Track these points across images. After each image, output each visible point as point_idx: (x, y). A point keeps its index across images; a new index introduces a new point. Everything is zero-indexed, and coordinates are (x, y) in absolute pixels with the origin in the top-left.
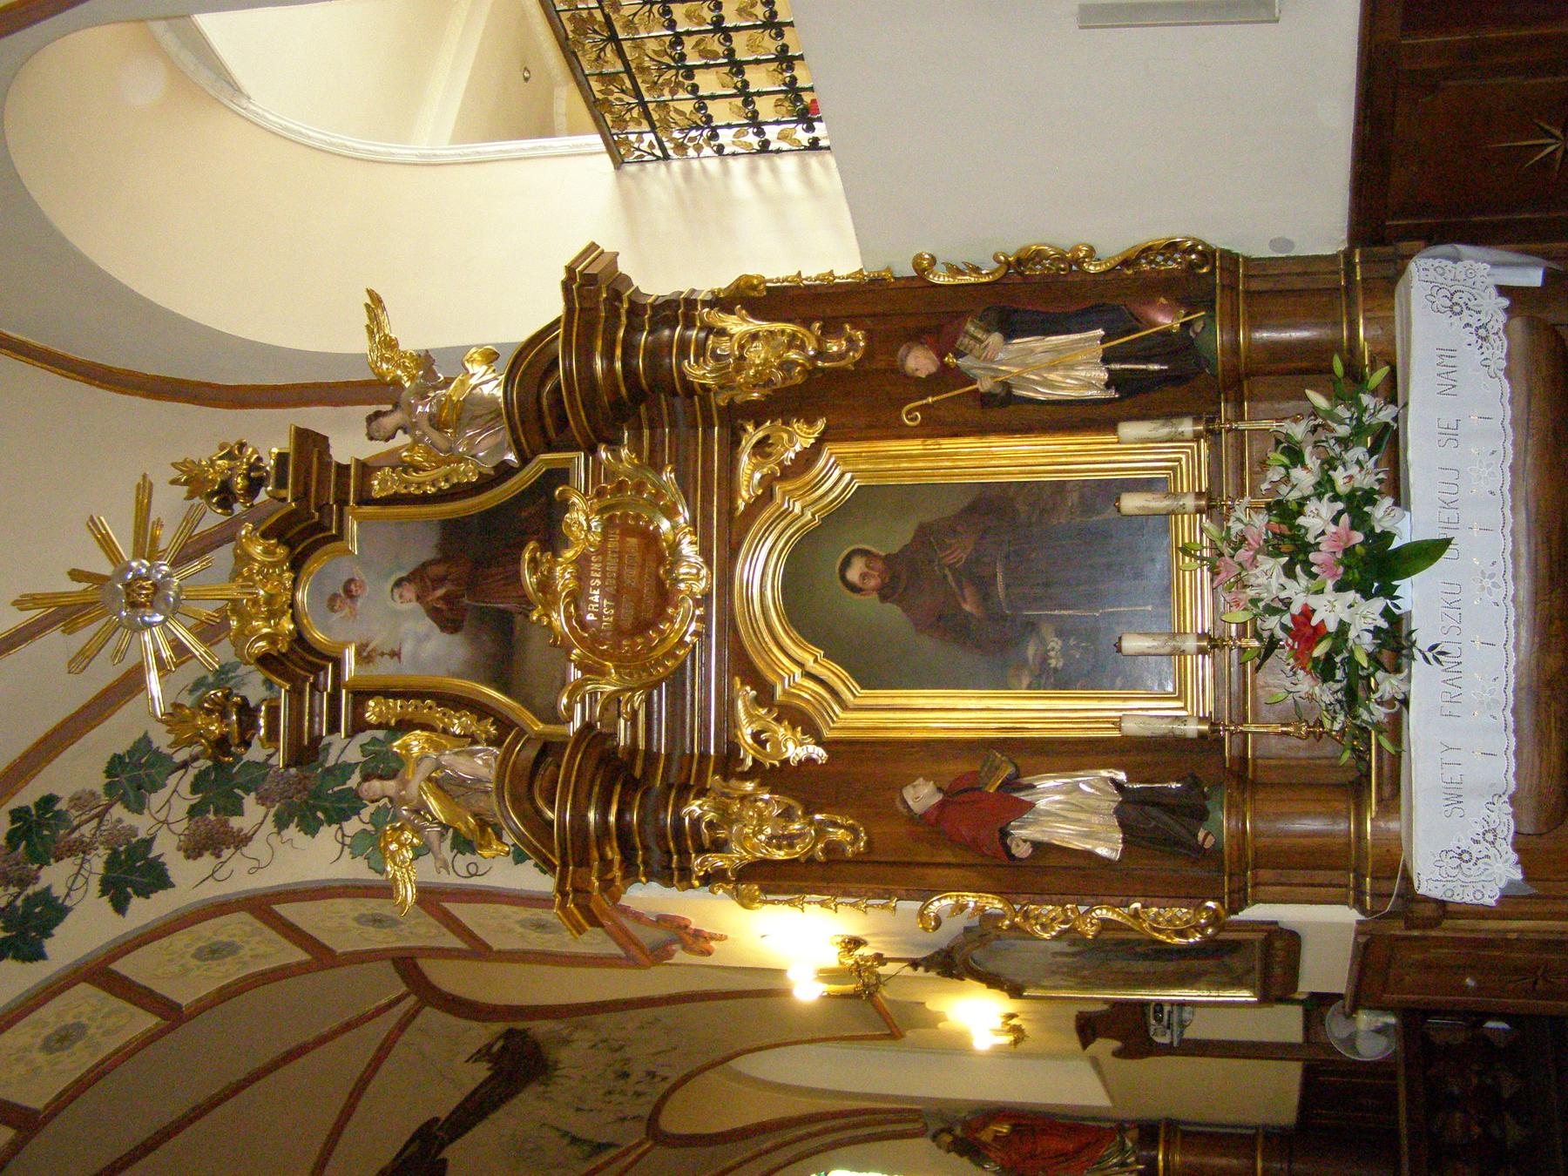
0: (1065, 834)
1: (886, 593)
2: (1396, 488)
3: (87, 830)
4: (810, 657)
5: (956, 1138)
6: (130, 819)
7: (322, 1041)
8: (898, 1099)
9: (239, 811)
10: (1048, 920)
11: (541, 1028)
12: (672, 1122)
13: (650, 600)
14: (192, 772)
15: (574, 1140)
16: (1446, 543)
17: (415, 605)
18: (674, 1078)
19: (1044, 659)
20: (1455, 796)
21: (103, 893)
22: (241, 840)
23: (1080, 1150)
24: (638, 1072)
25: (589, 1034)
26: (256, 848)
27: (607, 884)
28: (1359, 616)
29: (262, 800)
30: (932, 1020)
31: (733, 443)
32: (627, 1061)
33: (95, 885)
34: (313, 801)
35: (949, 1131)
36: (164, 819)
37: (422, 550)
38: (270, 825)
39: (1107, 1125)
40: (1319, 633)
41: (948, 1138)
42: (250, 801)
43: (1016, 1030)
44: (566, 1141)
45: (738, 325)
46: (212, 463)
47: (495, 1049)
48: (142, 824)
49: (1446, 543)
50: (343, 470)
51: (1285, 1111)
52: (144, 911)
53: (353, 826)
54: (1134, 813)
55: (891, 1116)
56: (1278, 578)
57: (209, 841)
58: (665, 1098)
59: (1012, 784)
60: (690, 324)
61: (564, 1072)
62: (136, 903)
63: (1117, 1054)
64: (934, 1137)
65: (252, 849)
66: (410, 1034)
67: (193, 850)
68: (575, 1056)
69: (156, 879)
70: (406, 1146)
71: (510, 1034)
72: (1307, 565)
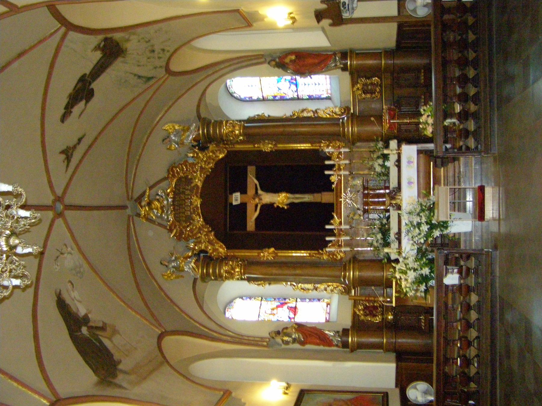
5: (276, 63)
7: (31, 48)
8: (256, 51)
11: (117, 36)
12: (174, 67)
15: (139, 77)
18: (172, 50)
23: (319, 63)
24: (157, 48)
25: (135, 37)
30: (261, 19)
32: (153, 46)
35: (274, 60)
39: (330, 53)
41: (273, 63)
43: (293, 18)
44: (136, 77)
47: (102, 45)
51: (392, 43)
55: (253, 58)
58: (169, 59)
61: (130, 52)
63: (331, 25)
64: (269, 63)
66: (66, 42)
68: (133, 45)
70: (77, 84)
71: (106, 39)
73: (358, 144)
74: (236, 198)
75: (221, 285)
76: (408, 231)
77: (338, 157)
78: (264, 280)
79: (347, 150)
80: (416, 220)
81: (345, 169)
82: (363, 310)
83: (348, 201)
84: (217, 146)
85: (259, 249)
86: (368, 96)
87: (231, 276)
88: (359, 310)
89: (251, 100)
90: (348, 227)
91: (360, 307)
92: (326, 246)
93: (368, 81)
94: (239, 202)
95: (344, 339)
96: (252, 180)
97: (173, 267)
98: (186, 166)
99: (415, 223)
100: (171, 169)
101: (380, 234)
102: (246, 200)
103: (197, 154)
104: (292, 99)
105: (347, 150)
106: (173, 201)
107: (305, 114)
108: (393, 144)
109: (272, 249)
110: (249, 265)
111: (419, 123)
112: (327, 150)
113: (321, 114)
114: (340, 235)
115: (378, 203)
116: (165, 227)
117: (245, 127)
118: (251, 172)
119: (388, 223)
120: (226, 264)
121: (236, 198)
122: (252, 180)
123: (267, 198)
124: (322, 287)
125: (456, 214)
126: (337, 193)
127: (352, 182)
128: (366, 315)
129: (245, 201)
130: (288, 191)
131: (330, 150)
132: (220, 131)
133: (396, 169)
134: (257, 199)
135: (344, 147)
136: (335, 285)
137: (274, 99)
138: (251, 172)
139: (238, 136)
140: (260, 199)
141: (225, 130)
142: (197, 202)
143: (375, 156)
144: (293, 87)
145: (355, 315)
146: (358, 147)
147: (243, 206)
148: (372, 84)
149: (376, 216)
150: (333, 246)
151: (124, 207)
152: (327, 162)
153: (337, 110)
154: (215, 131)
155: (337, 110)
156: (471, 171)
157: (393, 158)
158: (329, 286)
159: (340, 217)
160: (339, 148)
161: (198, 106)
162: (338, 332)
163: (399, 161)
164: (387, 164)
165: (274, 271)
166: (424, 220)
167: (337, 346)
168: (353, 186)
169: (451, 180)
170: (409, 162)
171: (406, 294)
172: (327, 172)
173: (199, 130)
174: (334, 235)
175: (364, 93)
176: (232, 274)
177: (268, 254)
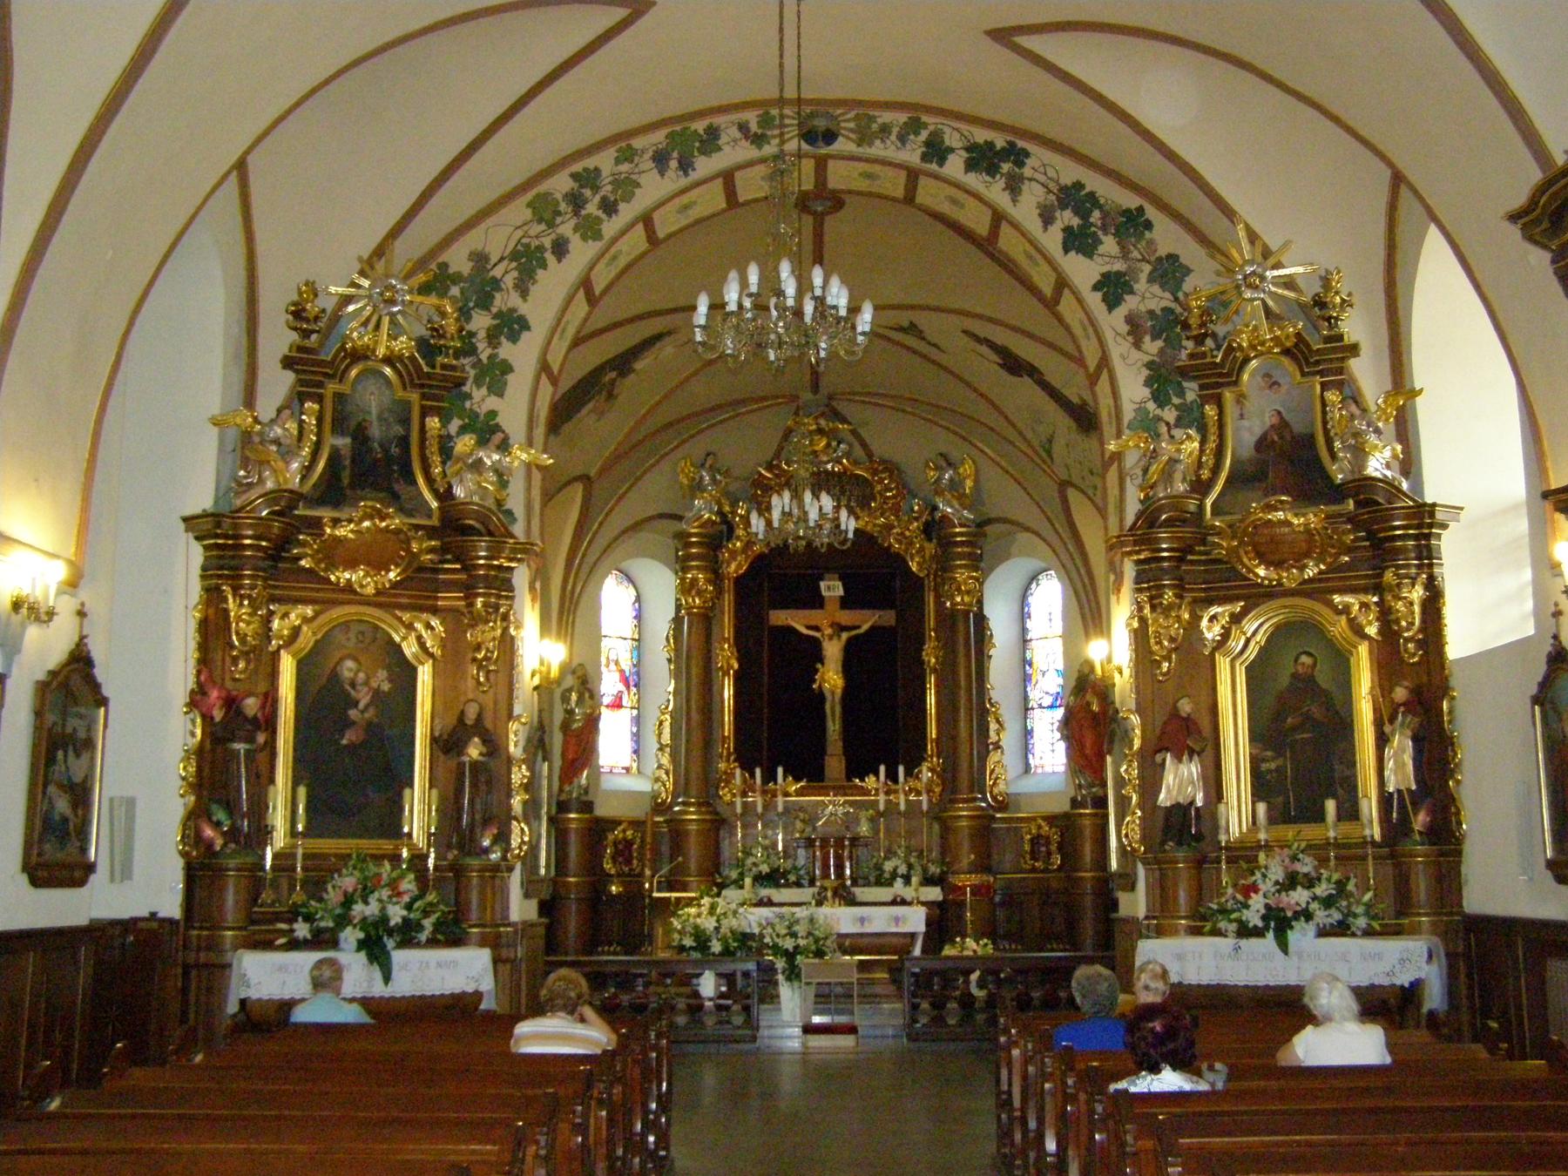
0: (1169, 778)
1: (1295, 676)
2: (1323, 933)
3: (1136, 254)
4: (1261, 638)
6: (1143, 277)
9: (1154, 338)
13: (1277, 558)
14: (1173, 305)
15: (1050, 441)
16: (1286, 953)
17: (1268, 424)
19: (1264, 760)
20: (1180, 957)
21: (1103, 275)
22: (1137, 344)
26: (1135, 355)
27: (1129, 554)
28: (1253, 917)
29: (1162, 352)
31: (1365, 590)
34: (1161, 380)
36: (1148, 297)
37: (1298, 427)
38: (1147, 358)
40: (1247, 896)
42: (1160, 343)
45: (1417, 594)
46: (1337, 293)
48: (1141, 285)
49: (1286, 953)
50: (1340, 371)
52: (1095, 300)
53: (1151, 406)
54: (1180, 813)
56: (1274, 878)
57: (1135, 327)
59: (1192, 752)
60: (1419, 567)
62: (1099, 295)
65: (1134, 351)
67: (1130, 320)
69: (1112, 303)
72: (1279, 891)
73: (936, 827)
74: (832, 588)
75: (667, 564)
76: (781, 917)
77: (911, 790)
78: (677, 650)
79: (925, 807)
80: (801, 929)
81: (888, 802)
82: (624, 839)
83: (832, 806)
85: (736, 638)
86: (1027, 847)
87: (686, 588)
88: (624, 831)
89: (1023, 615)
90: (780, 809)
91: (629, 833)
92: (743, 768)
93: (1054, 847)
95: (574, 805)
96: (866, 620)
97: (702, 478)
98: (894, 497)
99: (796, 928)
100: (891, 468)
101: (1124, 910)
102: (829, 607)
103: (916, 519)
104: (1026, 698)
105: (925, 807)
106: (826, 471)
107: (993, 726)
108: (934, 893)
109: (736, 666)
110: (707, 620)
111: (964, 936)
112: (924, 769)
113: (994, 757)
114: (764, 792)
115: (826, 866)
116: (777, 455)
117: (967, 613)
118: (887, 617)
119: (787, 885)
120: (708, 581)
121: (832, 588)
122: (866, 620)
123: (833, 650)
124: (665, 760)
125: (812, 991)
126: (843, 787)
127: (864, 816)
128: (615, 844)
131: (926, 775)
132: (960, 566)
133: (889, 898)
134: (830, 628)
135: (930, 801)
136: (670, 786)
137: (1026, 662)
138: (887, 617)
139: (952, 598)
140: (831, 638)
141: (961, 575)
143: (912, 860)
144: (1047, 701)
145: (615, 823)
146: (930, 827)
147: (817, 602)
148: (1049, 853)
149: (801, 861)
150: (744, 781)
151: (815, 387)
152: (901, 769)
153: (1002, 787)
154: (961, 556)
155: (1002, 787)
156: (883, 1021)
157: (908, 893)
158: (667, 773)
159: (799, 793)
160: (929, 791)
161: (1005, 521)
162: (586, 791)
163: (904, 902)
164: (899, 882)
165: (695, 671)
166: (802, 942)
167: (561, 790)
168: (857, 821)
169: (869, 990)
170: (897, 920)
171: (674, 914)
172: (882, 769)
173: (961, 525)
174: (765, 781)
175: (1032, 840)
176: (689, 592)
177: (726, 655)
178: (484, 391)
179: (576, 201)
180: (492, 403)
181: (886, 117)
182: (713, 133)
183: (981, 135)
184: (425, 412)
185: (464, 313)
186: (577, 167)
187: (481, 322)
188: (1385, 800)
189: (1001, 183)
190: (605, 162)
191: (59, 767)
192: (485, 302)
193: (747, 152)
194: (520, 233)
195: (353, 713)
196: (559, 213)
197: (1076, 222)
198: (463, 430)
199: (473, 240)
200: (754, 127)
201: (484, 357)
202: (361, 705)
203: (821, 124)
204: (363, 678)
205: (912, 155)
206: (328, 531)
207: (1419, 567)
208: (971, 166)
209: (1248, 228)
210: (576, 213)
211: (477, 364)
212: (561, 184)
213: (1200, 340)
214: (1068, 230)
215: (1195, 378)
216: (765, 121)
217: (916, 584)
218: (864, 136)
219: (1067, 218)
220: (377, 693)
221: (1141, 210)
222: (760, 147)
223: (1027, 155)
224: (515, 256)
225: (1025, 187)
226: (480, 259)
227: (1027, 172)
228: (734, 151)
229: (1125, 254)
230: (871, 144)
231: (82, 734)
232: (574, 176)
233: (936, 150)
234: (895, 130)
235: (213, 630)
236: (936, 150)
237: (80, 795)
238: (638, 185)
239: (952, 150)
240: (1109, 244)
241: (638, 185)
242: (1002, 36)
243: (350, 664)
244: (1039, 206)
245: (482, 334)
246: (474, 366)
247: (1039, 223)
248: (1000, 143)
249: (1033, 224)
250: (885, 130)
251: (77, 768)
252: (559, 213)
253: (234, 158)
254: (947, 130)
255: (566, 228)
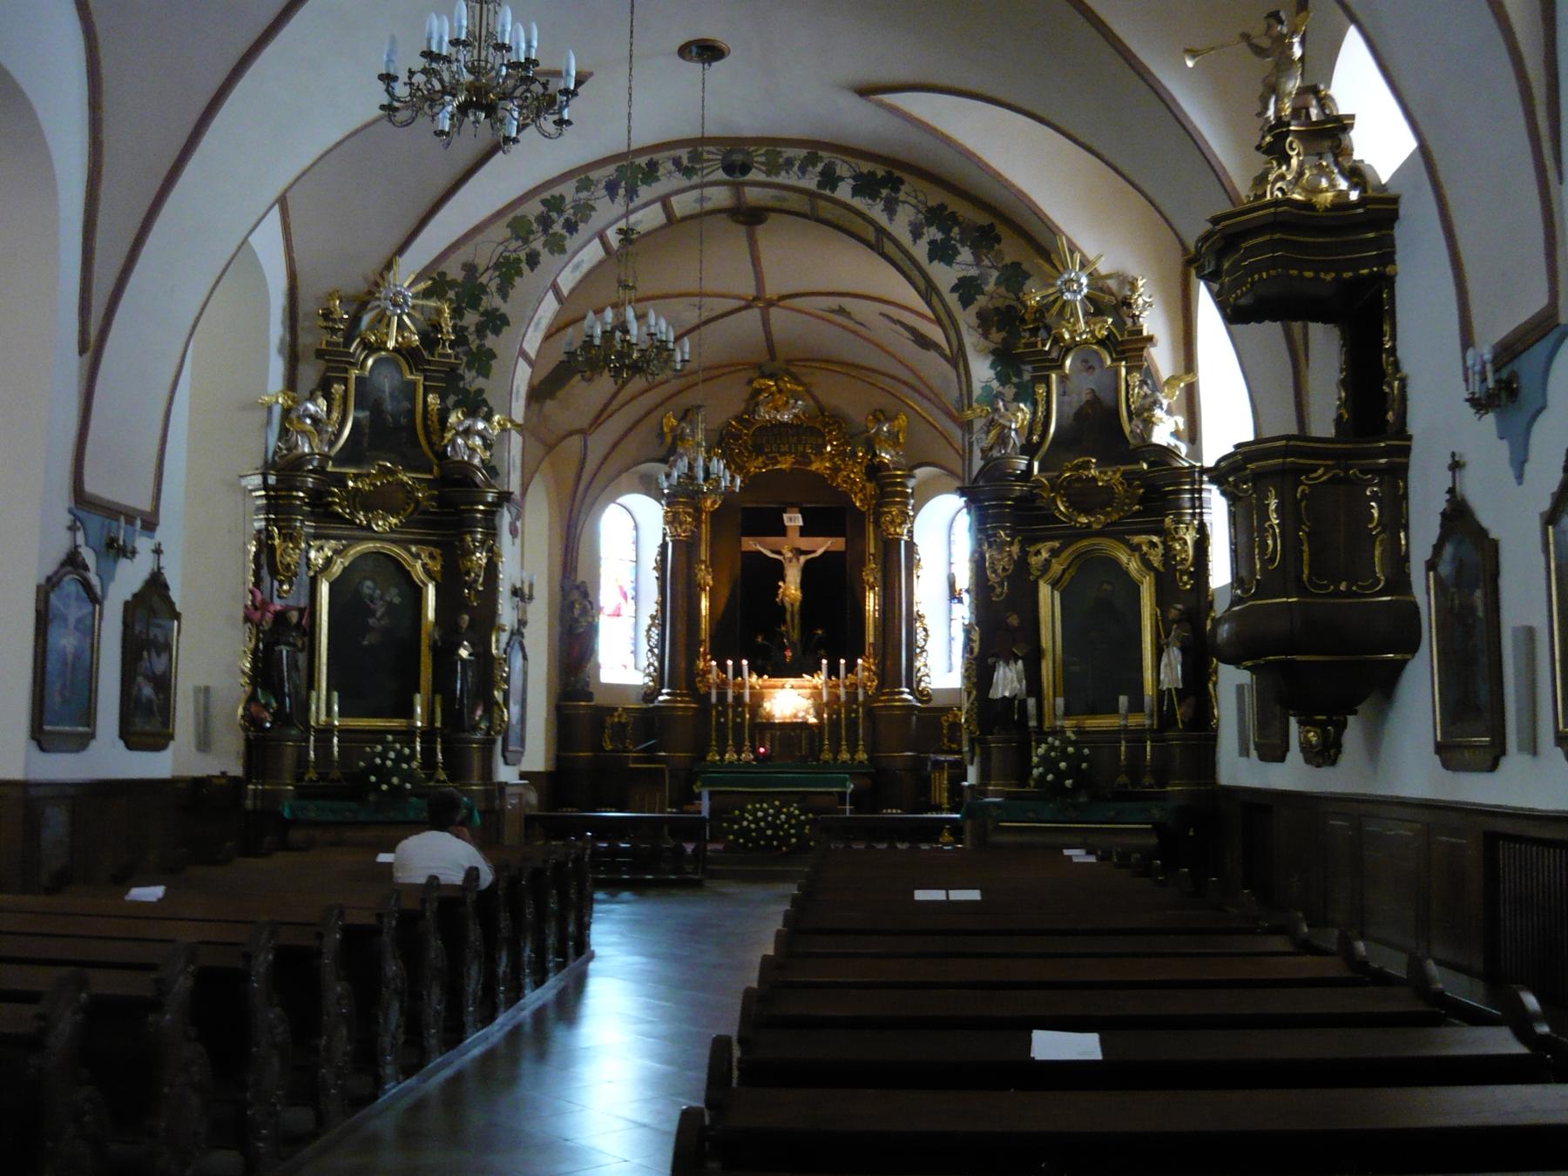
3: (986, 262)
6: (992, 281)
10: (599, 443)
22: (986, 335)
33: (961, 275)
38: (992, 346)
42: (1004, 334)
45: (1190, 537)
50: (346, 371)
52: (953, 300)
62: (956, 296)
67: (980, 315)
74: (794, 520)
84: (872, 497)
94: (787, 523)
96: (822, 545)
121: (794, 520)
122: (822, 545)
129: (790, 533)
130: (804, 602)
134: (794, 551)
142: (785, 464)
147: (782, 531)
178: (474, 373)
179: (545, 222)
180: (480, 382)
181: (789, 152)
182: (653, 166)
183: (866, 167)
184: (427, 390)
185: (457, 313)
186: (546, 195)
187: (471, 319)
188: (1160, 694)
189: (880, 205)
190: (568, 190)
191: (145, 664)
192: (474, 303)
193: (679, 181)
194: (501, 248)
195: (371, 621)
196: (532, 232)
197: (939, 236)
198: (457, 405)
199: (463, 255)
200: (685, 162)
201: (474, 347)
202: (379, 614)
203: (738, 158)
204: (380, 595)
205: (810, 182)
206: (351, 484)
207: (1193, 515)
208: (856, 191)
209: (1068, 240)
210: (545, 231)
211: (469, 353)
212: (534, 208)
213: (1034, 332)
214: (932, 243)
215: (1030, 363)
216: (695, 157)
217: (860, 516)
218: (773, 168)
219: (933, 233)
220: (390, 603)
221: (992, 226)
222: (689, 178)
223: (902, 182)
224: (497, 266)
225: (900, 208)
226: (470, 269)
227: (902, 196)
228: (668, 181)
229: (978, 262)
230: (777, 174)
231: (161, 639)
232: (544, 202)
233: (829, 179)
234: (797, 164)
235: (267, 561)
236: (829, 179)
237: (164, 684)
238: (593, 209)
239: (842, 179)
240: (965, 254)
241: (593, 209)
242: (866, 91)
243: (369, 583)
244: (911, 224)
245: (472, 329)
246: (465, 354)
247: (910, 237)
248: (880, 173)
249: (905, 238)
250: (789, 163)
251: (159, 665)
252: (532, 232)
253: (276, 194)
254: (839, 163)
255: (538, 244)
